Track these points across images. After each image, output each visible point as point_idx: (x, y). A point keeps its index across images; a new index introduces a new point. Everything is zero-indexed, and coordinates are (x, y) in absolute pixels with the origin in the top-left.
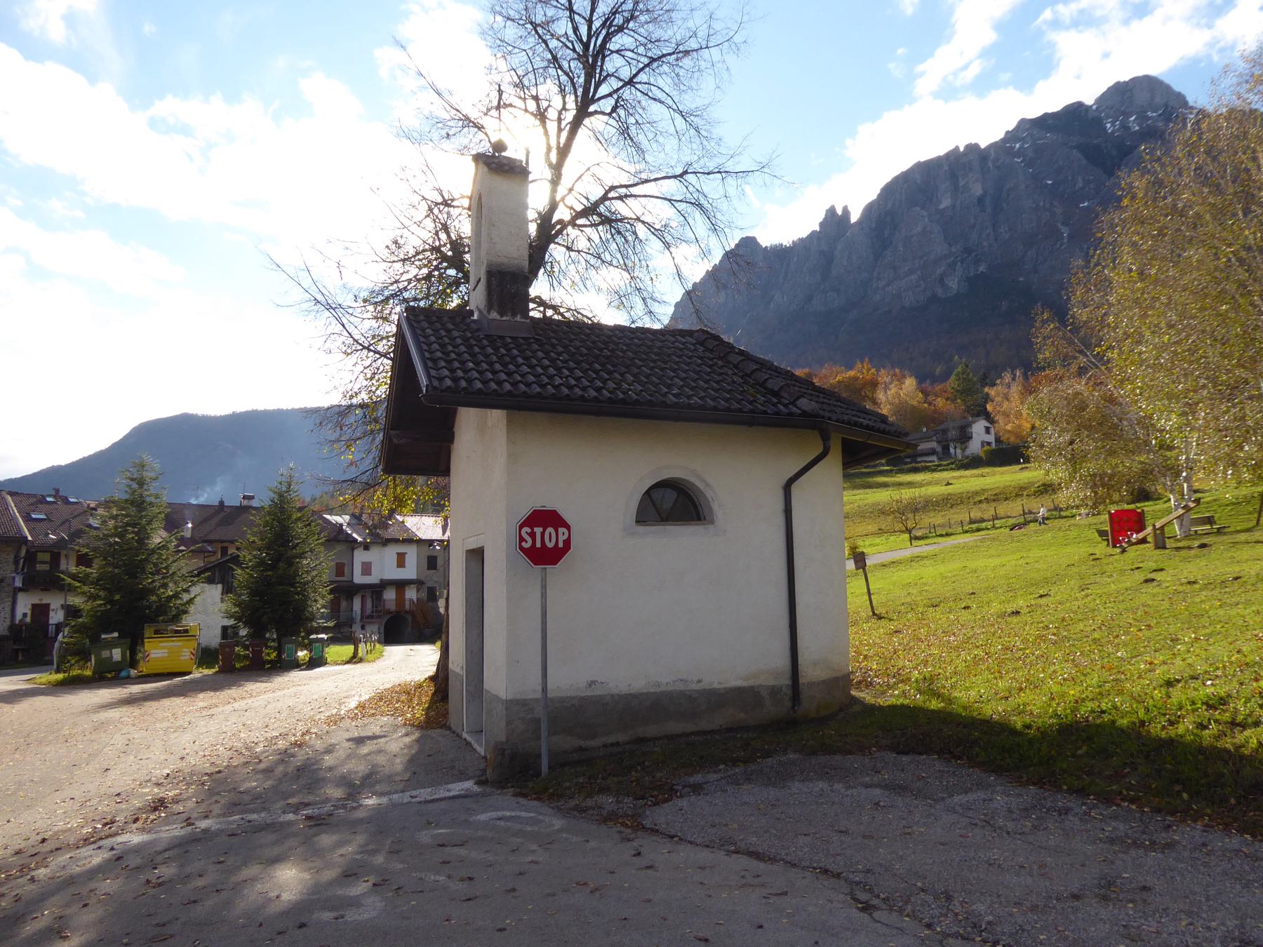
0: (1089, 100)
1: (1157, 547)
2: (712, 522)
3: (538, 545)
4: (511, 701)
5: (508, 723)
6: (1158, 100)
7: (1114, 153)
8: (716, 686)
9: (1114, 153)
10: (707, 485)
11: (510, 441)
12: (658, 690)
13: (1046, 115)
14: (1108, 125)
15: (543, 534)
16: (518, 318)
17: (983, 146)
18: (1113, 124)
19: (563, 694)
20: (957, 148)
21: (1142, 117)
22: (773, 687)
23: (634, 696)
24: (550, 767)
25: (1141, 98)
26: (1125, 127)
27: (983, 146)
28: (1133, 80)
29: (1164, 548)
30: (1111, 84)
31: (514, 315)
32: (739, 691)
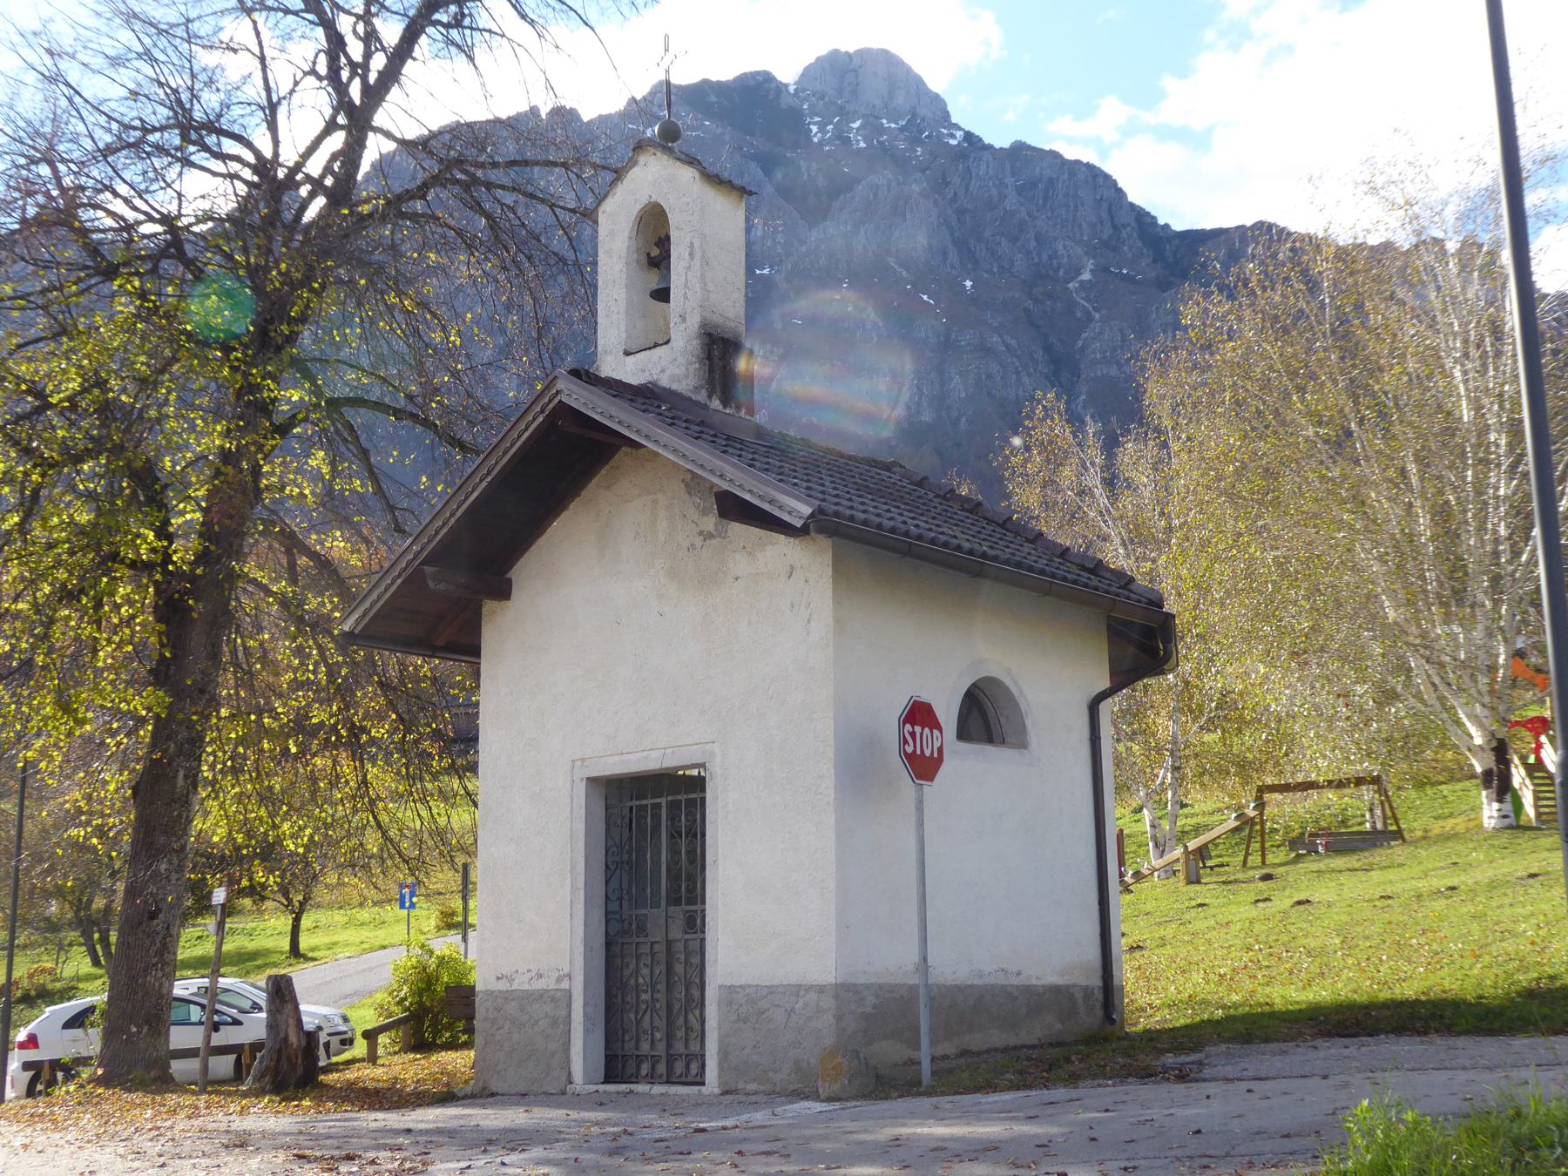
0: (787, 73)
1: (1190, 882)
2: (1022, 745)
8: (1034, 982)
11: (837, 601)
13: (706, 82)
14: (814, 129)
17: (586, 116)
18: (822, 129)
19: (891, 980)
20: (534, 111)
21: (872, 129)
22: (1087, 987)
23: (958, 988)
26: (842, 138)
27: (586, 116)
29: (1198, 882)
30: (823, 52)
32: (1055, 990)
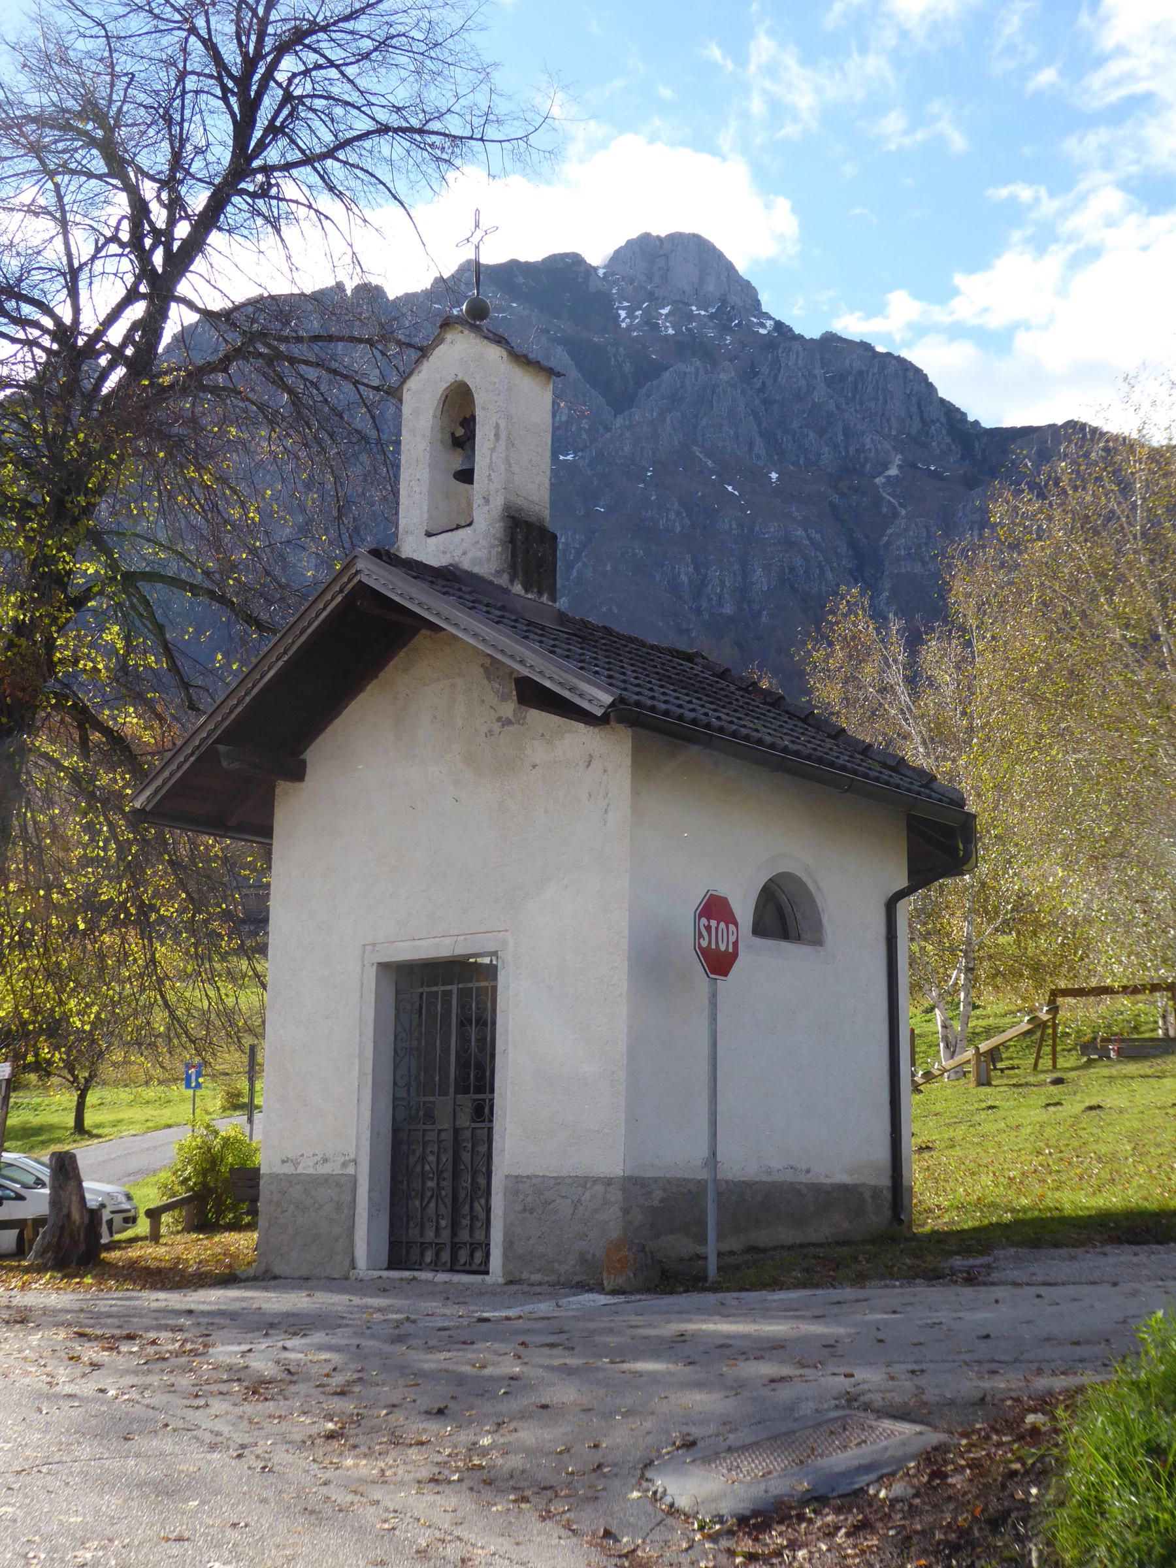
0: (597, 255)
1: (980, 1083)
3: (713, 946)
4: (630, 1178)
5: (626, 1211)
6: (711, 287)
7: (628, 367)
9: (628, 367)
10: (819, 889)
11: (636, 792)
12: (769, 1179)
13: (514, 263)
14: (623, 314)
15: (717, 928)
16: (544, 598)
18: (631, 312)
19: (680, 1175)
20: (340, 286)
21: (681, 314)
22: (876, 1187)
24: (719, 1269)
25: (684, 275)
28: (672, 237)
30: (634, 234)
31: (540, 593)
